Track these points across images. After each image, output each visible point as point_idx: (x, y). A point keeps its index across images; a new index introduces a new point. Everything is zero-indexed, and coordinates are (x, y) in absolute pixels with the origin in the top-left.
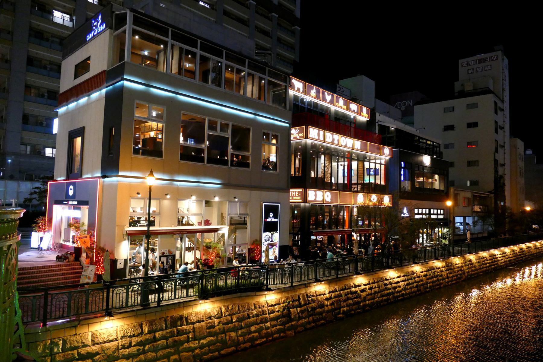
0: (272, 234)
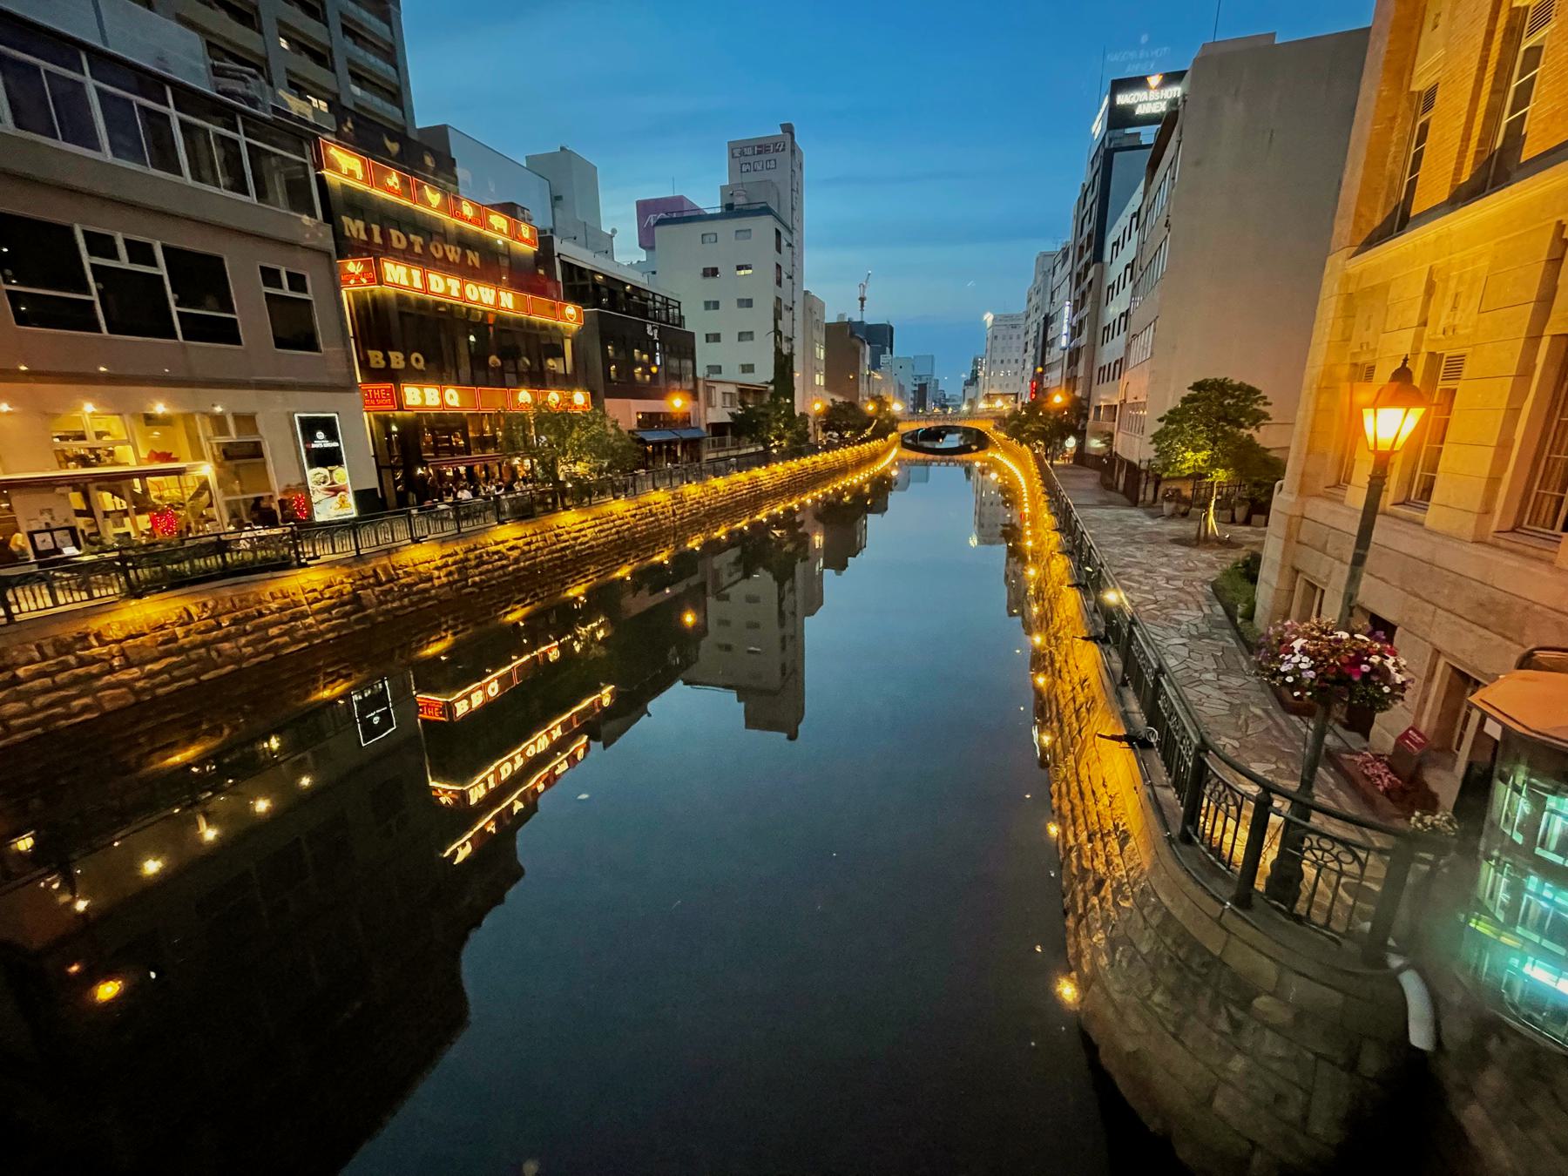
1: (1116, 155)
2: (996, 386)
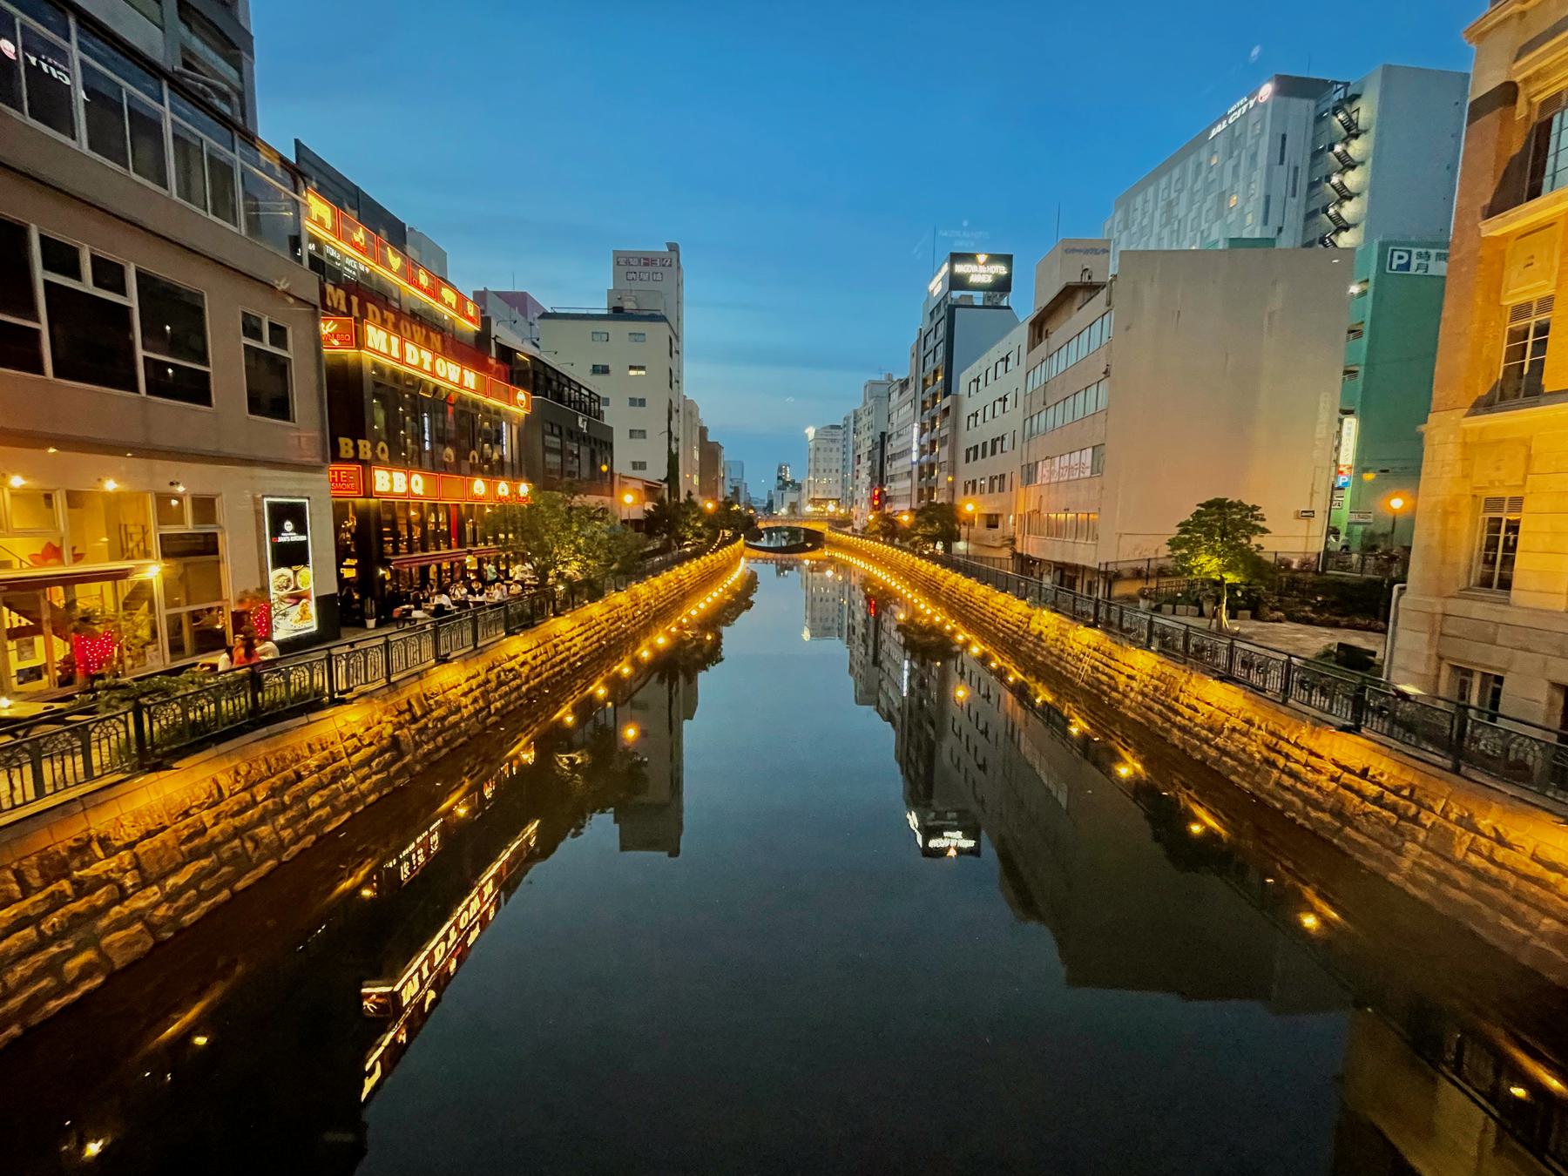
0: (295, 573)
1: (957, 310)
2: (820, 490)
